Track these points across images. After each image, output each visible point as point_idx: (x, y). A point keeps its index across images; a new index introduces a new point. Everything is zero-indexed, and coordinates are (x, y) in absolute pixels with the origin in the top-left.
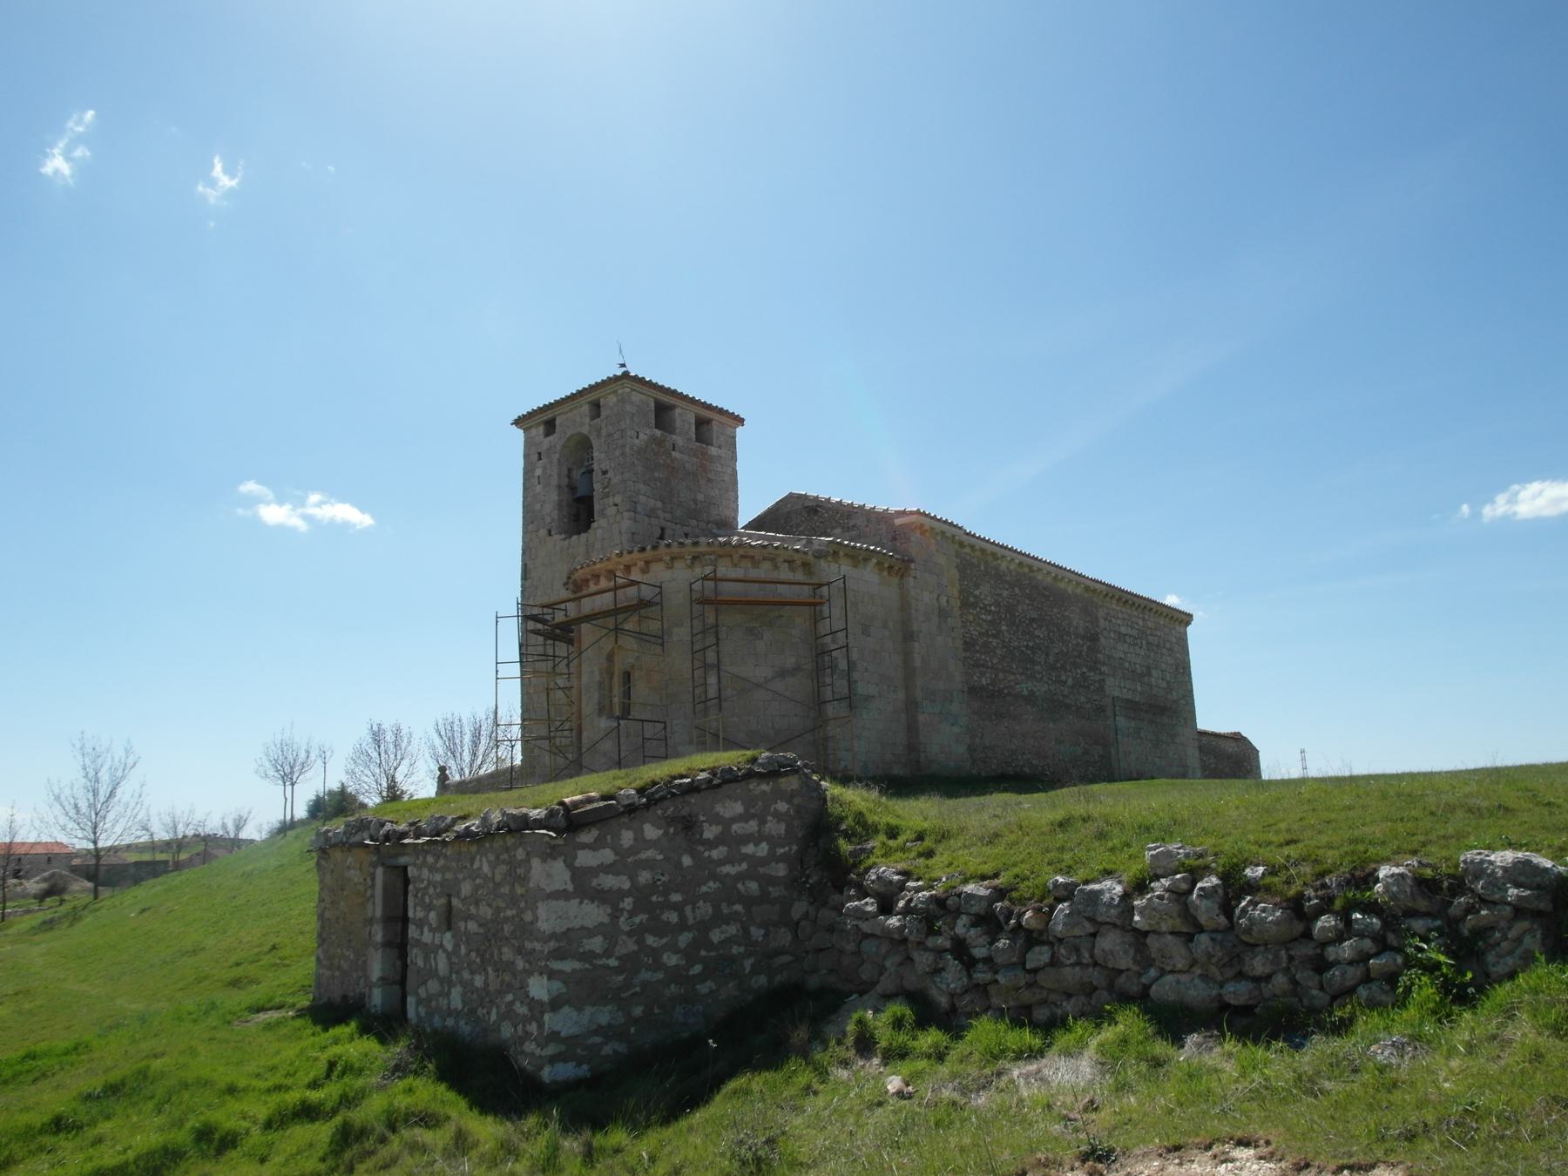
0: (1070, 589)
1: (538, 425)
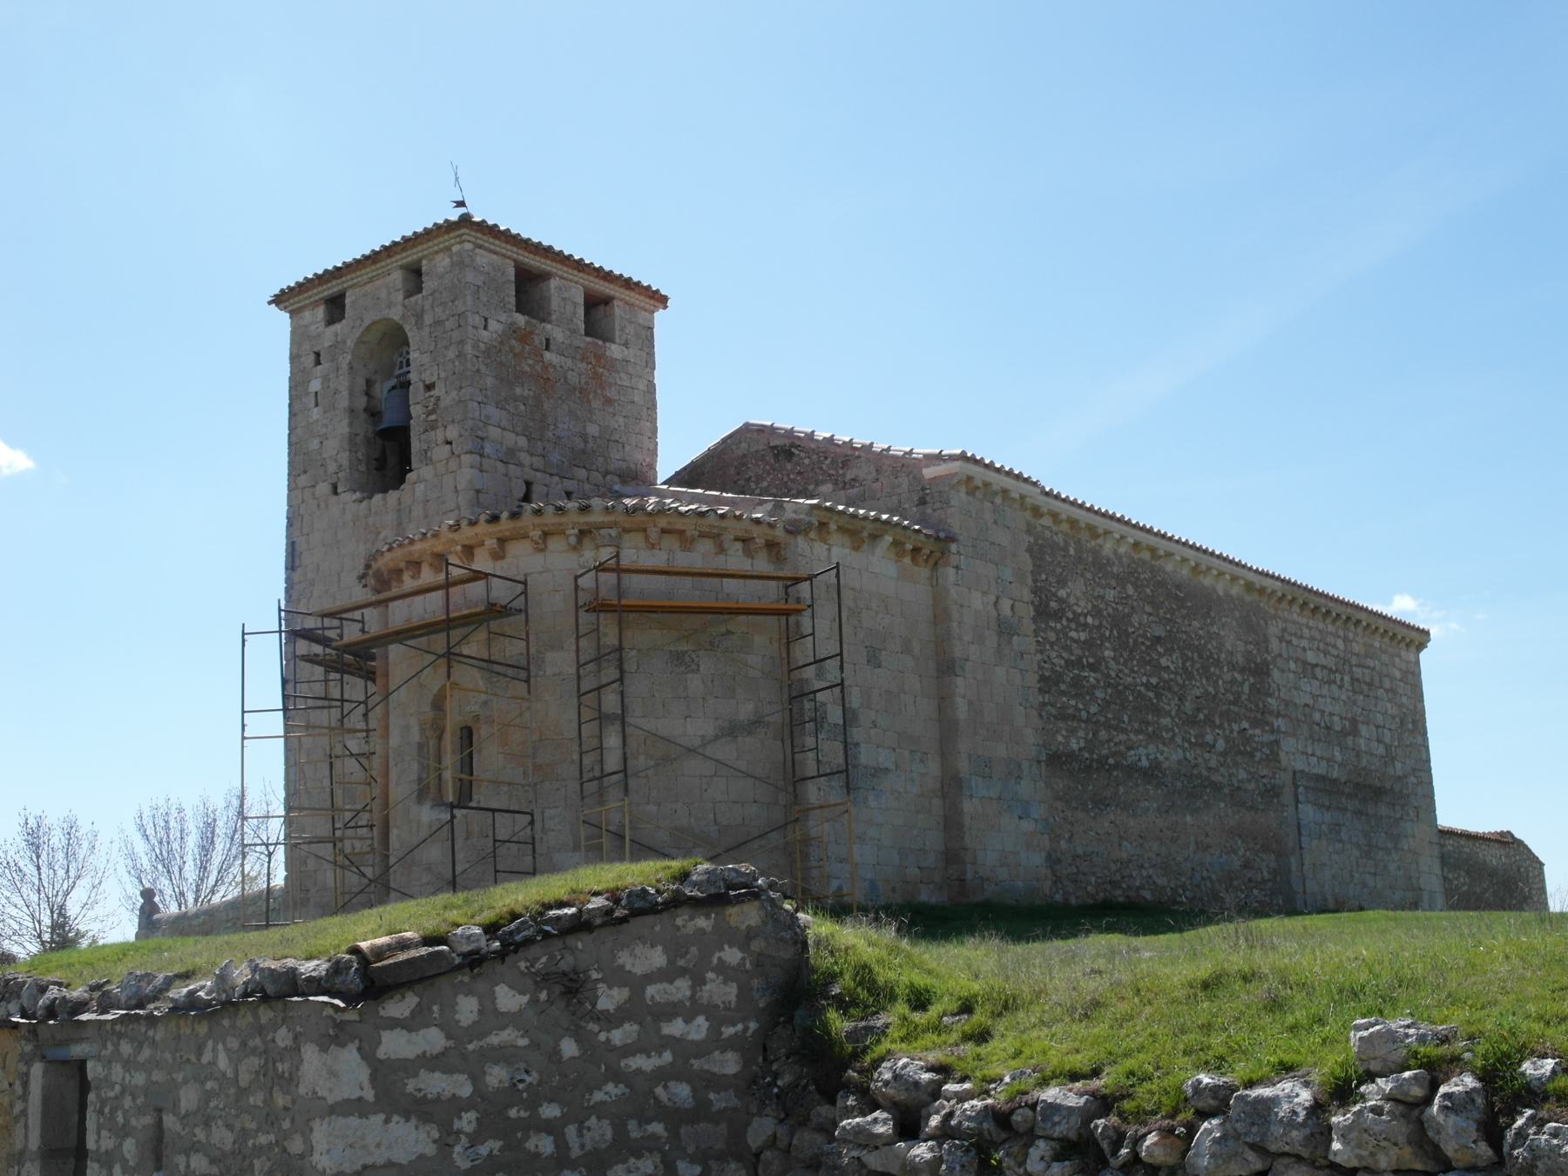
1: (315, 304)
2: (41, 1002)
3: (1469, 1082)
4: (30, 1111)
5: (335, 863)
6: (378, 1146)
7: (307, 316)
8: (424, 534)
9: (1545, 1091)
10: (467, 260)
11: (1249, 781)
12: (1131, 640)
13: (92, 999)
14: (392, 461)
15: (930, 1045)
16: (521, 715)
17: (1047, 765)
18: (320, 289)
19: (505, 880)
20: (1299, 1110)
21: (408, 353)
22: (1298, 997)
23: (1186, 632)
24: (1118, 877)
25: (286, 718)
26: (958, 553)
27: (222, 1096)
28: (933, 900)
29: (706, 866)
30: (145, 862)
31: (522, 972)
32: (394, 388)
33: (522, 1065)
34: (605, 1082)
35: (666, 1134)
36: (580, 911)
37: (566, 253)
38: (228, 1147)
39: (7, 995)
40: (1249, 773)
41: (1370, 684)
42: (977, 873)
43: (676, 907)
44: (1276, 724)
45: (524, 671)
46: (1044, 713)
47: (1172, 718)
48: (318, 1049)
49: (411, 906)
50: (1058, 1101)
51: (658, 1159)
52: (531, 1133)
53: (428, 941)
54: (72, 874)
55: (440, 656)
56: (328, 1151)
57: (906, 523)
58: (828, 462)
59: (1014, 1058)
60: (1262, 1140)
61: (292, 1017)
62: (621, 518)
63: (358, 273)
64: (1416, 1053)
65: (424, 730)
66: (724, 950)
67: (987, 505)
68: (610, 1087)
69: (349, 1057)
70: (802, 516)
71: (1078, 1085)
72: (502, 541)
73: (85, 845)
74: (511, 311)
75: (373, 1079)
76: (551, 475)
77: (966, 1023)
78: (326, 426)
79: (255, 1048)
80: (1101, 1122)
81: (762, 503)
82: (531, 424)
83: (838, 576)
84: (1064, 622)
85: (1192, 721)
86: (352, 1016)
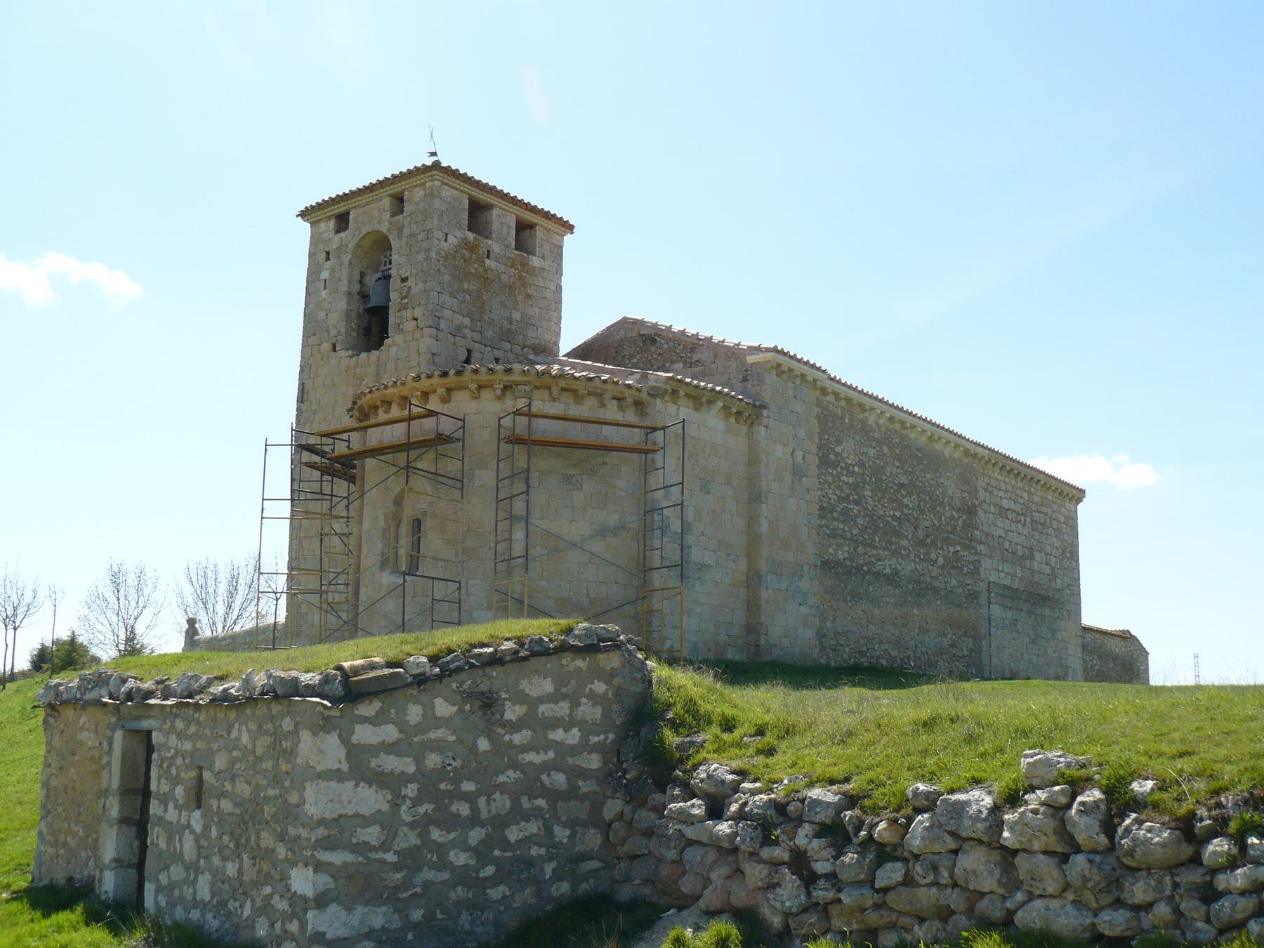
1: (329, 218)
2: (123, 689)
3: (1097, 794)
4: (113, 762)
5: (321, 608)
6: (350, 802)
7: (323, 225)
8: (395, 382)
9: (1146, 802)
10: (436, 193)
11: (958, 587)
12: (884, 485)
13: (157, 690)
14: (375, 330)
15: (734, 756)
16: (456, 513)
17: (821, 569)
18: (333, 208)
19: (439, 628)
20: (983, 809)
21: (390, 255)
22: (987, 735)
23: (921, 482)
24: (864, 649)
25: (292, 506)
26: (768, 417)
27: (244, 761)
28: (737, 658)
29: (585, 624)
30: (190, 600)
31: (453, 690)
32: (379, 279)
33: (450, 754)
34: (507, 769)
35: (547, 807)
36: (496, 650)
37: (505, 192)
38: (247, 796)
39: (100, 683)
40: (958, 581)
41: (1043, 525)
42: (767, 641)
43: (562, 652)
44: (979, 549)
45: (460, 482)
46: (821, 532)
47: (909, 541)
48: (311, 734)
49: (378, 641)
50: (820, 798)
51: (541, 824)
52: (455, 801)
53: (390, 665)
54: (141, 604)
55: (401, 469)
56: (316, 803)
57: (733, 393)
58: (680, 347)
59: (791, 768)
60: (957, 829)
61: (294, 711)
62: (533, 379)
63: (360, 198)
64: (1064, 774)
65: (388, 519)
66: (594, 683)
67: (790, 384)
68: (510, 773)
69: (332, 742)
70: (660, 385)
71: (835, 787)
72: (449, 390)
73: (150, 585)
74: (464, 229)
75: (348, 756)
76: (486, 346)
77: (759, 742)
78: (331, 303)
79: (268, 730)
80: (849, 813)
81: (632, 374)
82: (474, 309)
83: (683, 428)
84: (839, 470)
85: (922, 543)
86: (336, 713)
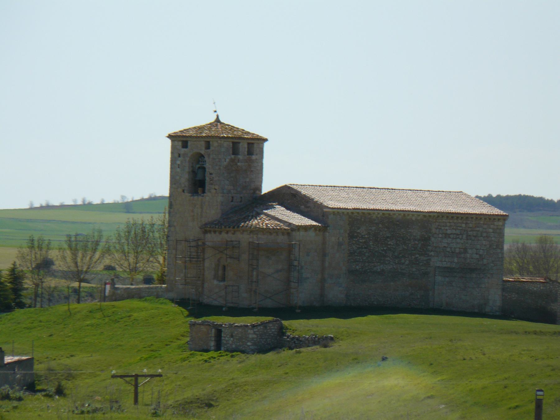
0: (414, 218)
1: (179, 141)
